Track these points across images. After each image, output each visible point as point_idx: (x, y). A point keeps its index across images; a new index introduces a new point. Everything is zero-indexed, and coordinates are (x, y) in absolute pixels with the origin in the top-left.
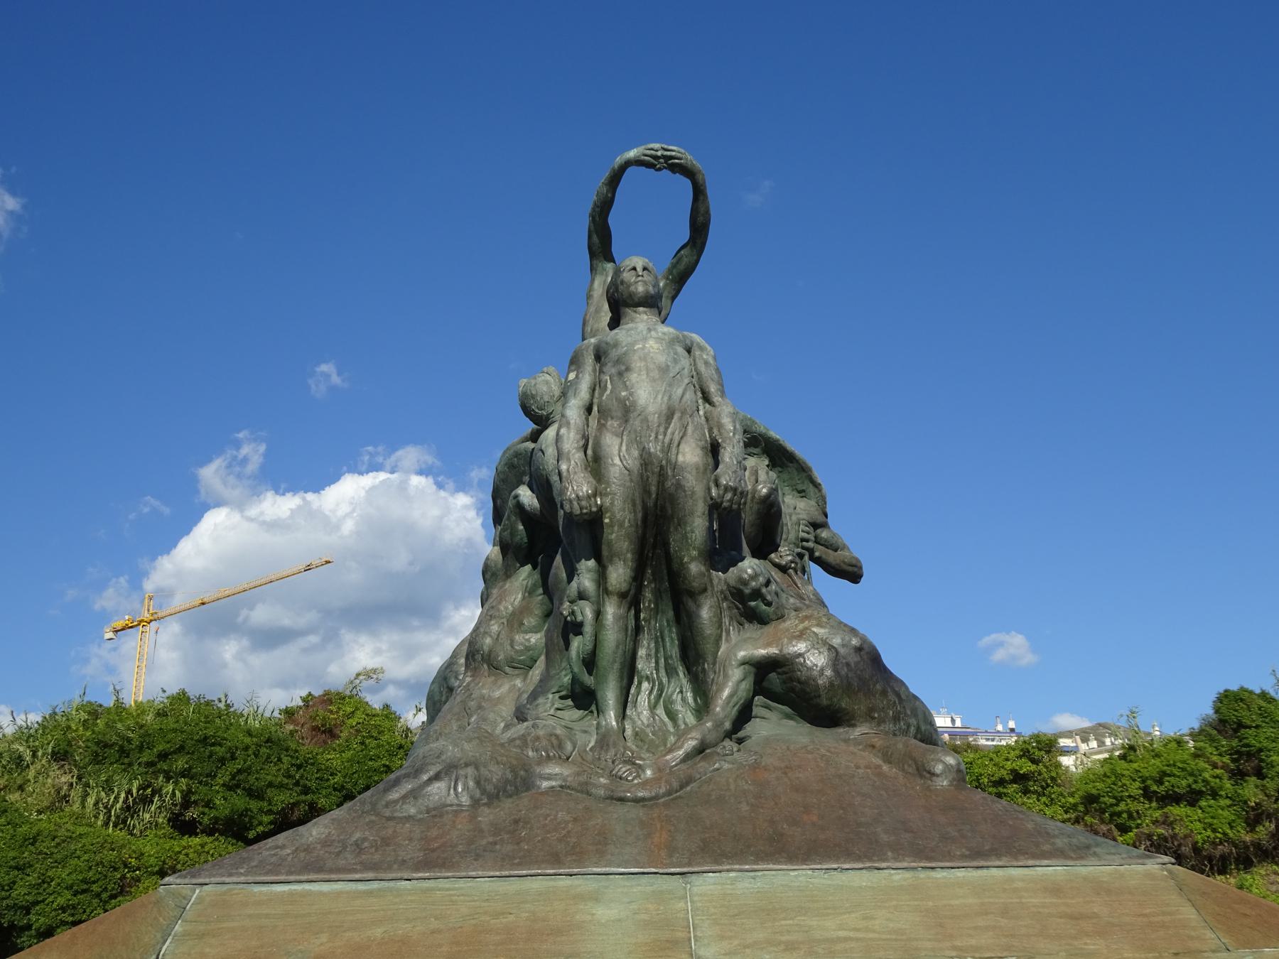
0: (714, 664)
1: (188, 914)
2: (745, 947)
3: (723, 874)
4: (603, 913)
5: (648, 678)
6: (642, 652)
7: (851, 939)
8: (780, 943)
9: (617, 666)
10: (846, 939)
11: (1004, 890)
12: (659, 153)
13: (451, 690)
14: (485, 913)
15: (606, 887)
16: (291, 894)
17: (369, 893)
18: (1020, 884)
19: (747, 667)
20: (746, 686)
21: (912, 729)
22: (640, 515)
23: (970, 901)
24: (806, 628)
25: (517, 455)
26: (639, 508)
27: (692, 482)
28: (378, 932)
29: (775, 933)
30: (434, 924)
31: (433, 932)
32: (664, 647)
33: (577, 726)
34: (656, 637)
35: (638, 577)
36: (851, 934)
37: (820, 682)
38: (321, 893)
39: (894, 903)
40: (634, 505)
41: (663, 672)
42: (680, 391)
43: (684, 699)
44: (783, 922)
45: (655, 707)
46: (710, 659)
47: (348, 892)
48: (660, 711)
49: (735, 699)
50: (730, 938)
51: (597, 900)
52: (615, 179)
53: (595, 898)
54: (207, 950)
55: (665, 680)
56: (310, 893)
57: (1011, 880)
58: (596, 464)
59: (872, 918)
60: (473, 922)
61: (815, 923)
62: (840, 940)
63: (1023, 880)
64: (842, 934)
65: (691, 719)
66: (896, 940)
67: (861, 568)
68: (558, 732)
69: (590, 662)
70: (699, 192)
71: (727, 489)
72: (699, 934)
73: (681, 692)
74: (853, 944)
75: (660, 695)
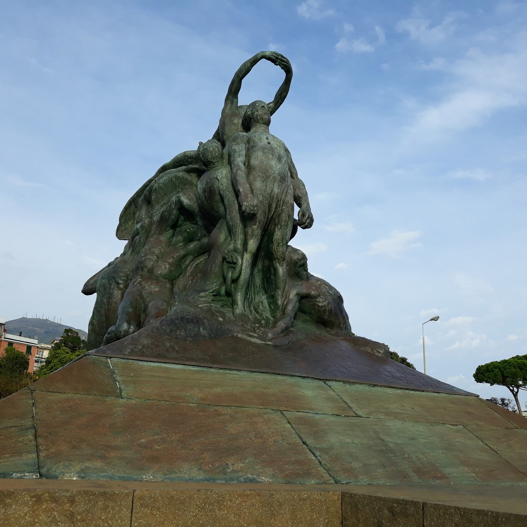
12: (280, 57)
35: (259, 249)
52: (254, 61)
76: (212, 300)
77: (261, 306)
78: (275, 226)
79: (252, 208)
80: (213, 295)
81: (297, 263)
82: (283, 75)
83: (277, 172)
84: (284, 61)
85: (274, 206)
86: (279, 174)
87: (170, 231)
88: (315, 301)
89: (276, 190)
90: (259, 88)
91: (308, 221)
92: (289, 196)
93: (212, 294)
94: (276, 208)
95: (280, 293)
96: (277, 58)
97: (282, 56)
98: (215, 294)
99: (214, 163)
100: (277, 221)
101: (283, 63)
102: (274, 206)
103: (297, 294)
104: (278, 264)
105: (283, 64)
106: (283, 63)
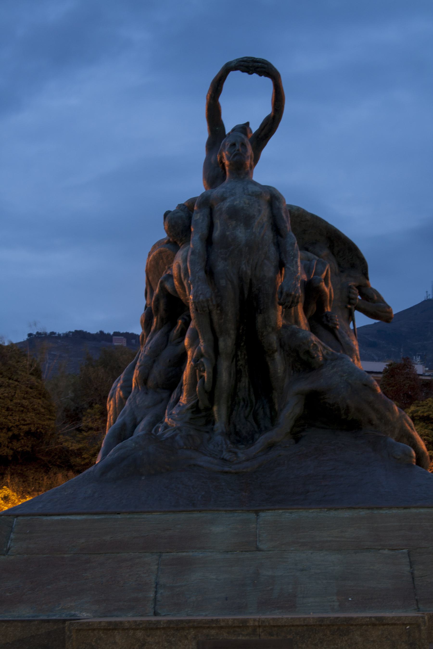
3: (276, 511)
12: (251, 64)
35: (237, 345)
52: (227, 70)
68: (192, 433)
72: (261, 539)
90: (245, 106)
93: (191, 411)
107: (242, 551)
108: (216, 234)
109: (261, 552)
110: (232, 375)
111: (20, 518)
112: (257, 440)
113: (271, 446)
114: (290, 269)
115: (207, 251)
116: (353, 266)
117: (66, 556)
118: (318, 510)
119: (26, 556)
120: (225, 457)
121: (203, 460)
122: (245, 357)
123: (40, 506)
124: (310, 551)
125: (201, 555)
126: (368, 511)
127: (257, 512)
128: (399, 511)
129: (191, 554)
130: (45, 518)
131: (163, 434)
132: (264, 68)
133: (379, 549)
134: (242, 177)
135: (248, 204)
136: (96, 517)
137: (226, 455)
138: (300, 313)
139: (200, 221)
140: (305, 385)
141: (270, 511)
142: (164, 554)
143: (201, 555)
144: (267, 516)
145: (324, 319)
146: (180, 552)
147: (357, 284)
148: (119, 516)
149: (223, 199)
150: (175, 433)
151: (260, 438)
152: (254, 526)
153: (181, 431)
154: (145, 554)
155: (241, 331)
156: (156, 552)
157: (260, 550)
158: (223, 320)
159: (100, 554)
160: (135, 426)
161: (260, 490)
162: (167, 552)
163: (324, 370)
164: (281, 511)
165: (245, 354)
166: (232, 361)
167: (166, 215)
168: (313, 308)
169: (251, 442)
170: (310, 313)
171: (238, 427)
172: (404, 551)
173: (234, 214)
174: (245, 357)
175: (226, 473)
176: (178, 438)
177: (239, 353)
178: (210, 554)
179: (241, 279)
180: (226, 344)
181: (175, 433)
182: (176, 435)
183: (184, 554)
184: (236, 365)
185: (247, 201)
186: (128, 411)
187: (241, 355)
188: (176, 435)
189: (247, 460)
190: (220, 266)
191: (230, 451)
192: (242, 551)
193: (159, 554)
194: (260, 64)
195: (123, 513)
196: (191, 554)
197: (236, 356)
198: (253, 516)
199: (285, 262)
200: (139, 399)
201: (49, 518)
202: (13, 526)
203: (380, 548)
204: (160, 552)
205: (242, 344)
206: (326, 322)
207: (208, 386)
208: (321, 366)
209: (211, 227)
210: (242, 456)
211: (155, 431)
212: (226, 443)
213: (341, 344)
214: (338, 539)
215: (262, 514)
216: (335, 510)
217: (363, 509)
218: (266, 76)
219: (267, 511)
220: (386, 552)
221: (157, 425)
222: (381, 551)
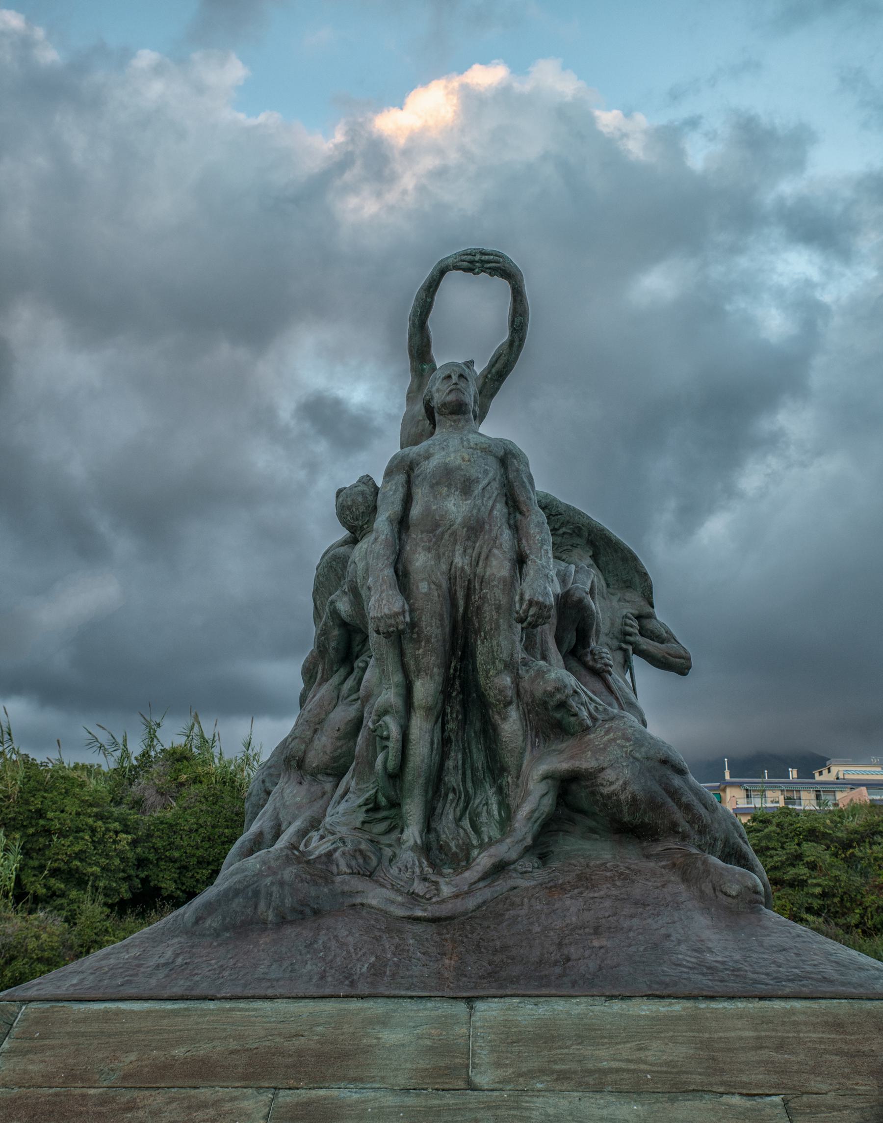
0: (518, 778)
1: (15, 1031)
2: (520, 1075)
3: (507, 1000)
4: (390, 1037)
5: (454, 790)
6: (450, 763)
7: (624, 1070)
8: (553, 1072)
9: (421, 781)
10: (618, 1071)
11: (783, 1023)
12: (477, 258)
13: (268, 793)
14: (280, 1035)
15: (395, 1011)
16: (106, 1011)
17: (175, 1013)
18: (802, 1018)
19: (549, 781)
20: (548, 803)
21: (720, 845)
22: (447, 629)
23: (747, 1034)
24: (610, 741)
25: (335, 558)
26: (447, 622)
27: (495, 594)
28: (179, 1052)
29: (550, 1061)
30: (233, 1045)
31: (231, 1053)
32: (471, 757)
33: (385, 840)
34: (464, 749)
35: (446, 693)
36: (623, 1065)
37: (622, 797)
38: (133, 1012)
39: (670, 1034)
40: (442, 619)
41: (469, 784)
42: (491, 503)
43: (489, 812)
44: (559, 1051)
45: (460, 819)
46: (513, 772)
47: (157, 1011)
48: (466, 823)
49: (536, 815)
50: (506, 1066)
51: (384, 1024)
52: (442, 272)
53: (384, 1022)
54: (31, 1067)
55: (471, 791)
56: (118, 1013)
57: (792, 1012)
58: (402, 577)
59: (646, 1049)
60: (268, 1044)
61: (588, 1053)
62: (611, 1071)
63: (804, 1013)
64: (615, 1065)
65: (495, 833)
66: (666, 1072)
67: (689, 659)
68: (363, 846)
69: (396, 776)
70: (518, 294)
71: (531, 603)
72: (477, 1061)
73: (487, 804)
74: (626, 1076)
75: (465, 808)
76: (363, 823)
77: (484, 814)
78: (476, 635)
79: (389, 621)
80: (367, 811)
81: (545, 703)
82: (502, 285)
83: (459, 520)
84: (489, 262)
85: (460, 595)
86: (464, 524)
87: (342, 670)
88: (593, 785)
89: (459, 561)
91: (531, 612)
92: (494, 563)
93: (364, 808)
94: (468, 597)
95: (510, 779)
96: (471, 262)
97: (483, 253)
98: (371, 806)
99: (362, 527)
100: (477, 625)
101: (489, 265)
102: (460, 595)
103: (545, 777)
104: (497, 717)
105: (490, 268)
106: (489, 265)
107: (437, 1089)
108: (416, 511)
109: (476, 1093)
110: (435, 746)
111: (33, 1005)
112: (474, 860)
113: (500, 868)
114: (535, 562)
115: (400, 539)
116: (628, 585)
117: (92, 1091)
118: (589, 999)
119: (16, 1090)
120: (416, 891)
121: (375, 896)
122: (457, 716)
123: (75, 981)
124: (576, 1094)
125: (355, 1096)
126: (689, 1004)
127: (469, 1000)
128: (750, 1005)
129: (334, 1093)
130: (76, 1006)
131: (316, 848)
132: (498, 262)
133: (722, 1094)
134: (460, 425)
135: (469, 461)
136: (169, 1006)
137: (419, 887)
138: (550, 644)
139: (391, 493)
140: (558, 761)
141: (496, 1000)
142: (282, 1093)
143: (355, 1096)
144: (490, 1010)
145: (589, 658)
146: (314, 1088)
147: (636, 612)
148: (211, 1005)
149: (427, 457)
150: (334, 846)
151: (481, 856)
152: (464, 1030)
153: (344, 843)
154: (245, 1090)
155: (452, 671)
156: (268, 1088)
157: (475, 1089)
158: (421, 650)
159: (159, 1088)
160: (277, 836)
161: (478, 954)
162: (290, 1089)
163: (592, 736)
164: (516, 1000)
165: (458, 712)
166: (436, 722)
167: (339, 492)
168: (571, 638)
169: (464, 863)
170: (565, 647)
171: (443, 837)
172: (774, 1098)
173: (447, 476)
174: (457, 716)
175: (418, 919)
176: (337, 854)
177: (449, 710)
178: (373, 1094)
179: (452, 580)
180: (425, 689)
181: (334, 846)
182: (335, 850)
183: (322, 1092)
184: (443, 730)
185: (467, 457)
186: (270, 811)
187: (452, 713)
188: (335, 850)
189: (456, 896)
190: (420, 560)
191: (425, 879)
192: (437, 1089)
193: (273, 1091)
194: (492, 257)
195: (219, 999)
196: (334, 1093)
197: (443, 713)
198: (461, 1008)
199: (528, 552)
200: (288, 791)
201: (83, 1006)
202: (15, 1025)
203: (721, 1090)
204: (275, 1088)
205: (454, 694)
206: (591, 663)
207: (391, 764)
208: (586, 730)
209: (408, 501)
210: (446, 891)
211: (306, 846)
212: (421, 866)
213: (617, 699)
214: (632, 1066)
215: (480, 1005)
216: (622, 999)
217: (677, 998)
218: (502, 276)
219: (490, 1000)
220: (736, 1100)
221: (310, 834)
222: (725, 1099)
